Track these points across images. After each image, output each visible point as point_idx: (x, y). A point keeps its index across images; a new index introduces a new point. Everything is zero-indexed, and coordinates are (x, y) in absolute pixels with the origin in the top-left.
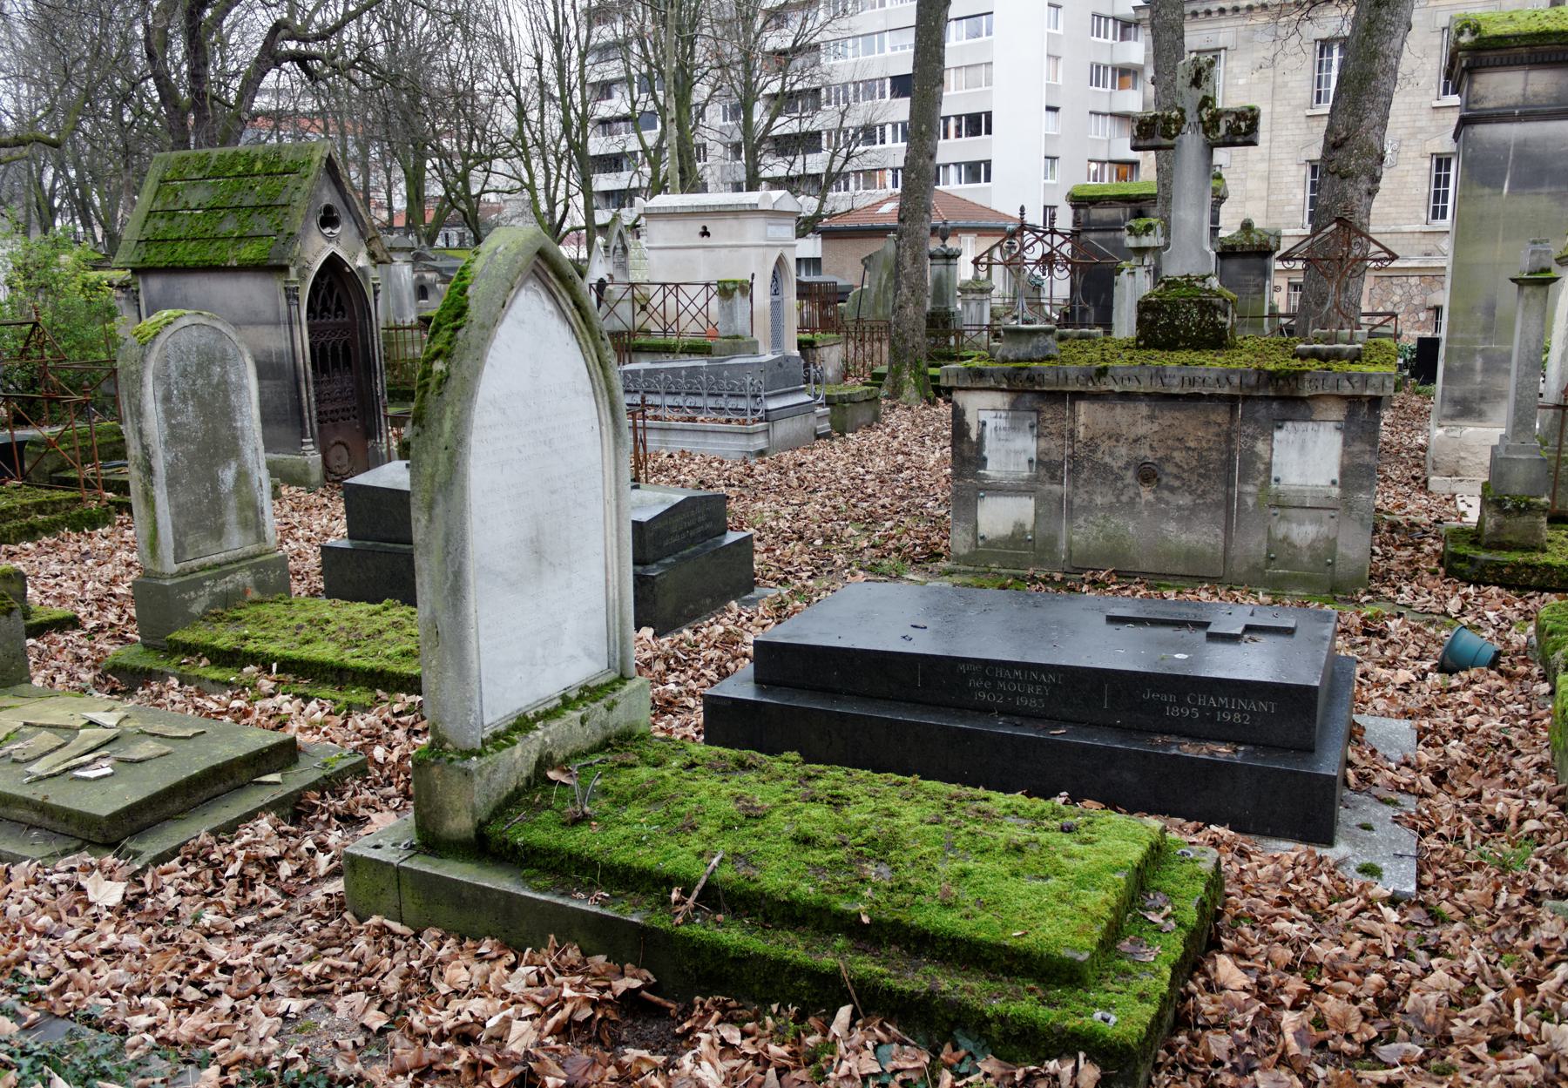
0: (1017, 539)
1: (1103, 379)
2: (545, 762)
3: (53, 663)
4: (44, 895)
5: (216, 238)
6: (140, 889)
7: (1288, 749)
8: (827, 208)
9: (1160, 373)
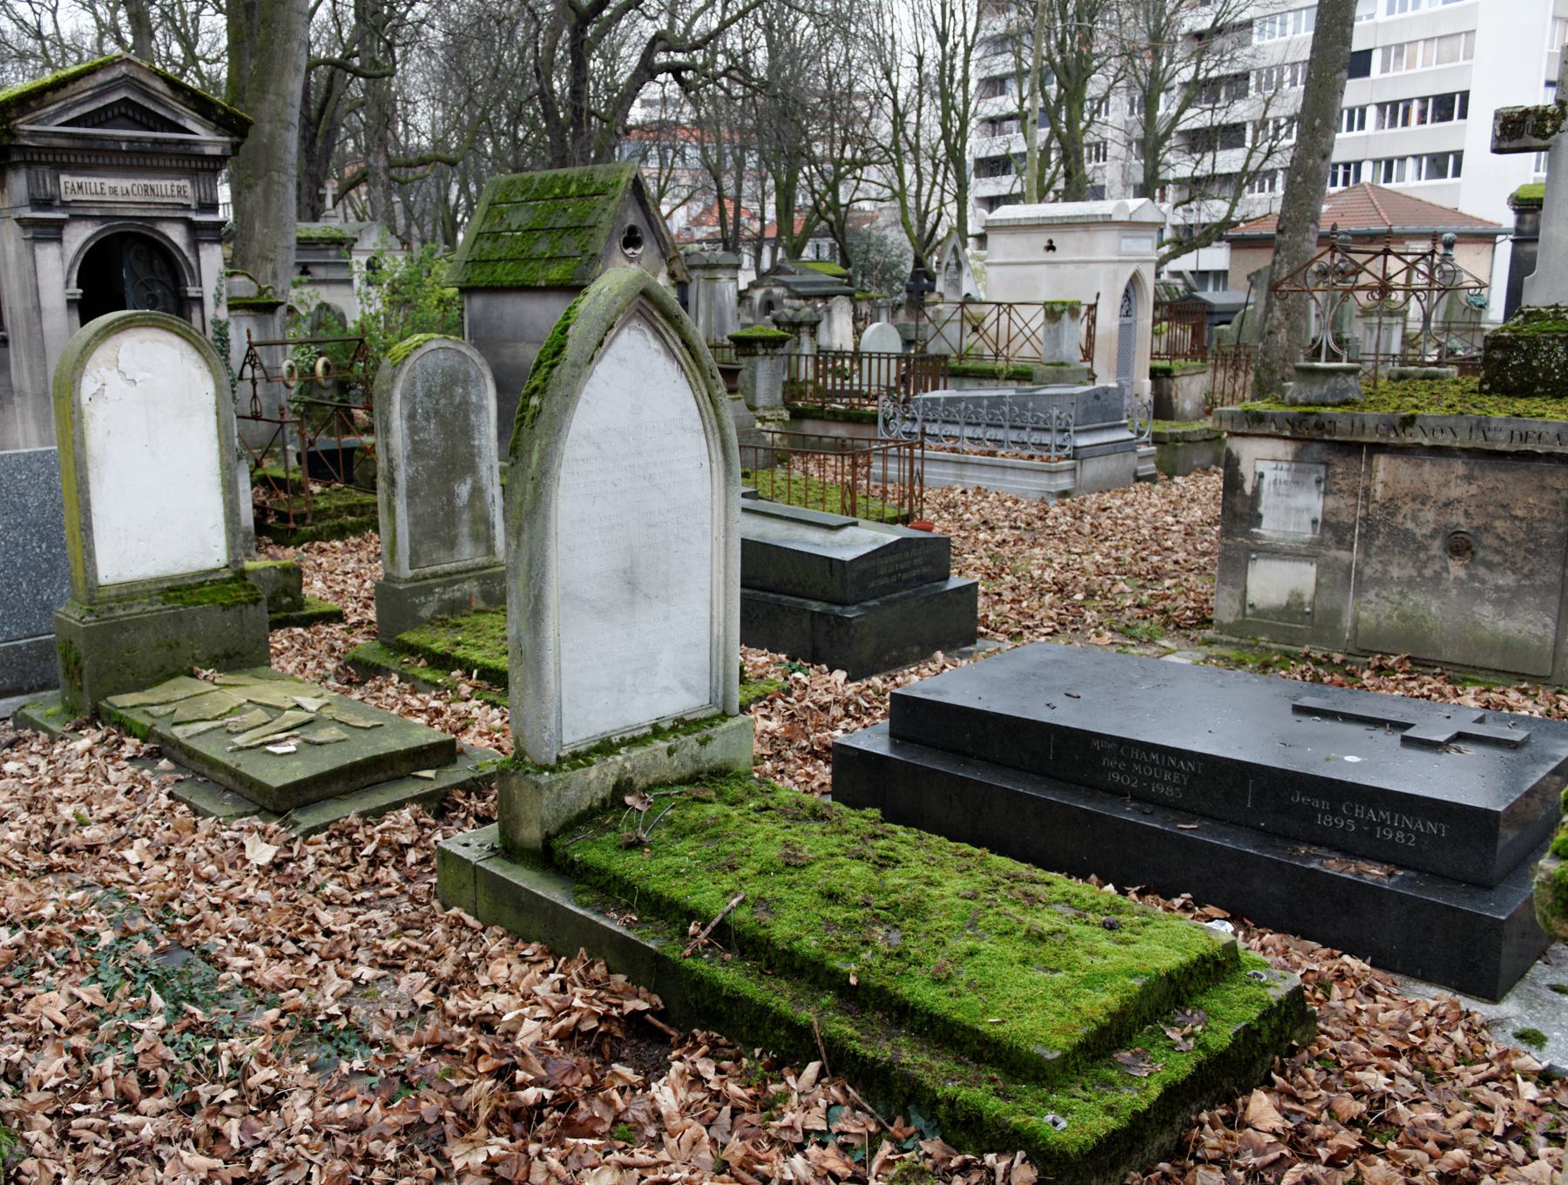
0: (1292, 610)
1: (1409, 430)
2: (623, 787)
3: (311, 651)
4: (215, 848)
5: (530, 259)
6: (288, 855)
7: (1460, 882)
8: (1238, 214)
9: (1482, 426)
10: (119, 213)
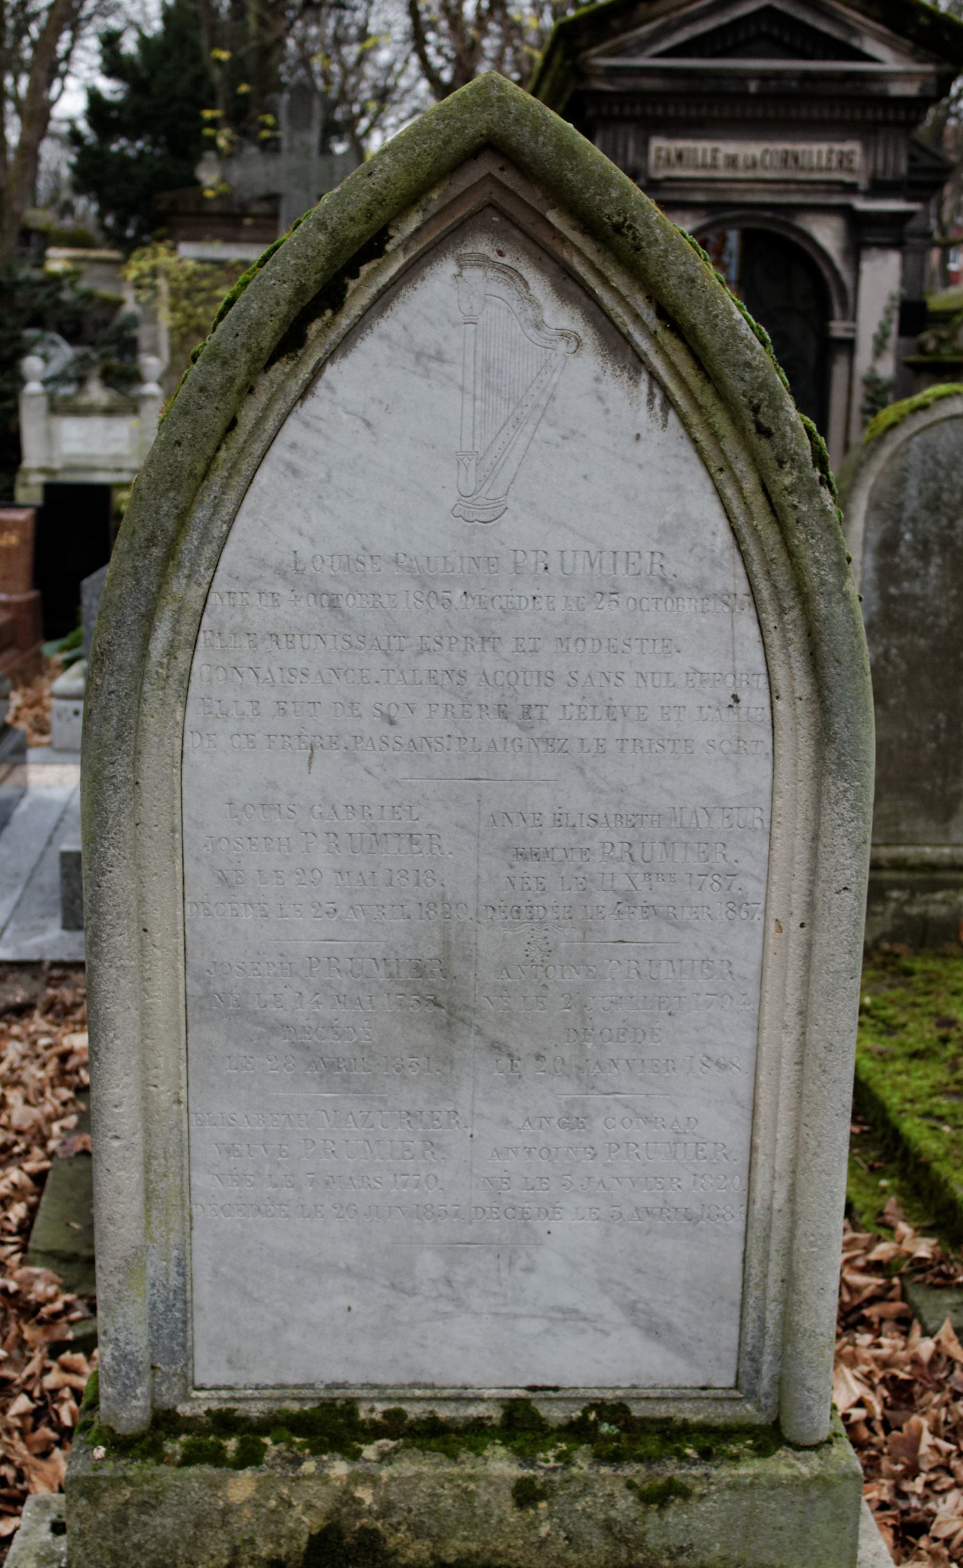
10: (736, 198)
